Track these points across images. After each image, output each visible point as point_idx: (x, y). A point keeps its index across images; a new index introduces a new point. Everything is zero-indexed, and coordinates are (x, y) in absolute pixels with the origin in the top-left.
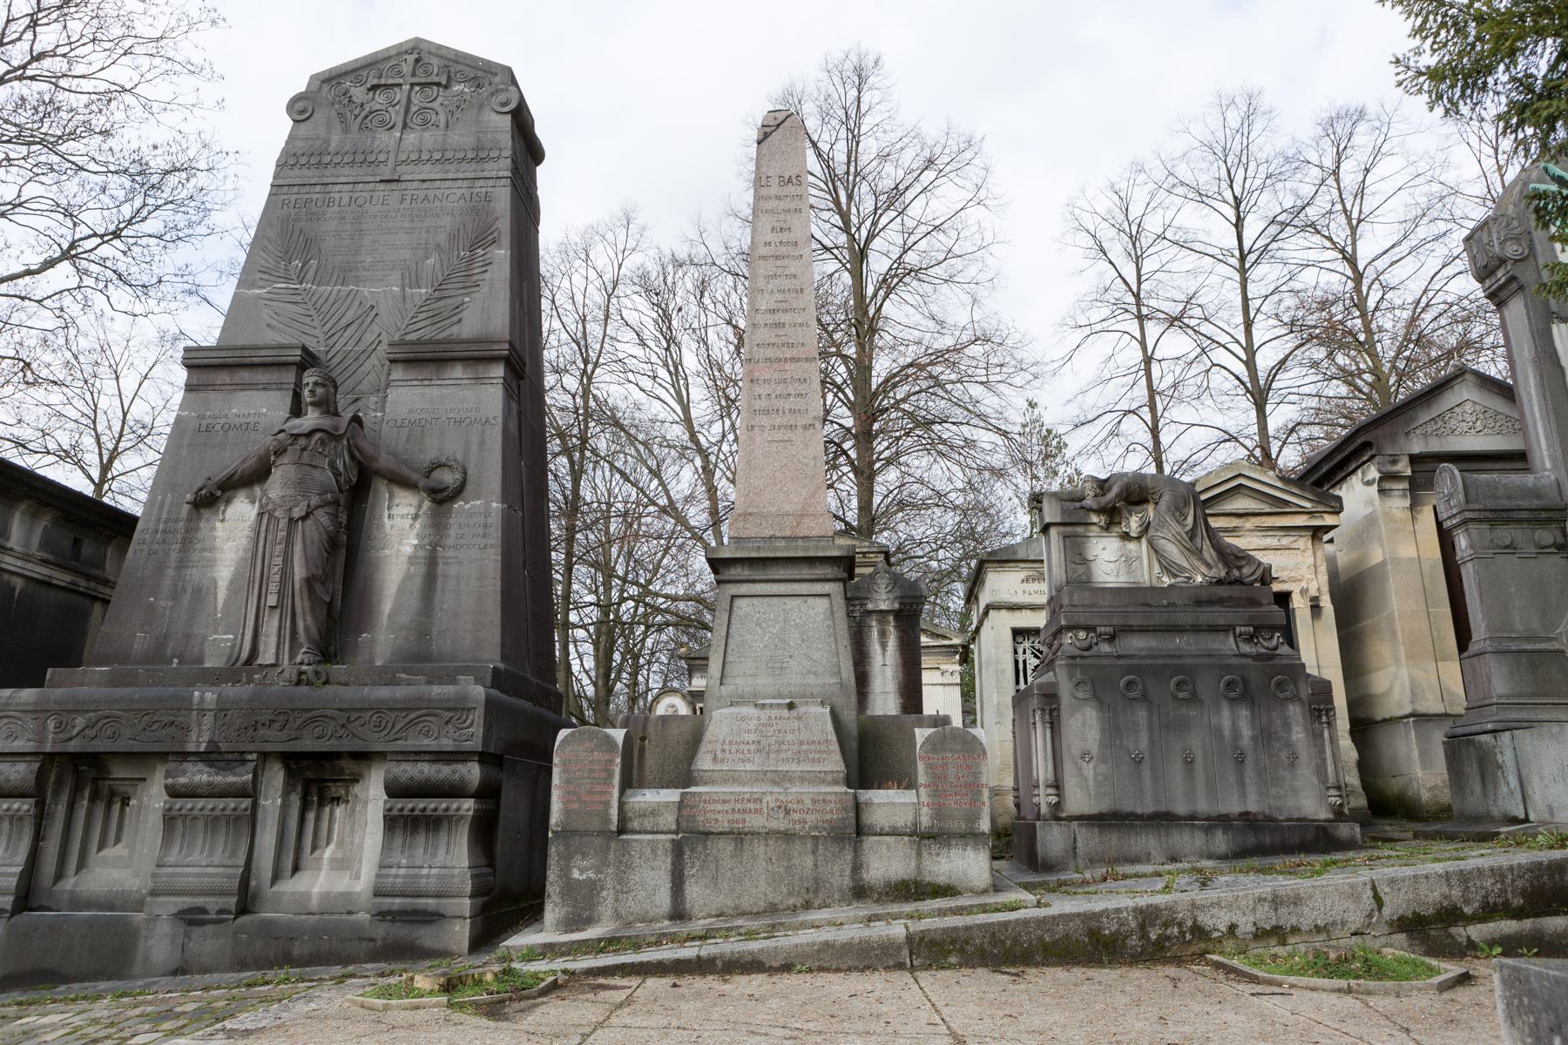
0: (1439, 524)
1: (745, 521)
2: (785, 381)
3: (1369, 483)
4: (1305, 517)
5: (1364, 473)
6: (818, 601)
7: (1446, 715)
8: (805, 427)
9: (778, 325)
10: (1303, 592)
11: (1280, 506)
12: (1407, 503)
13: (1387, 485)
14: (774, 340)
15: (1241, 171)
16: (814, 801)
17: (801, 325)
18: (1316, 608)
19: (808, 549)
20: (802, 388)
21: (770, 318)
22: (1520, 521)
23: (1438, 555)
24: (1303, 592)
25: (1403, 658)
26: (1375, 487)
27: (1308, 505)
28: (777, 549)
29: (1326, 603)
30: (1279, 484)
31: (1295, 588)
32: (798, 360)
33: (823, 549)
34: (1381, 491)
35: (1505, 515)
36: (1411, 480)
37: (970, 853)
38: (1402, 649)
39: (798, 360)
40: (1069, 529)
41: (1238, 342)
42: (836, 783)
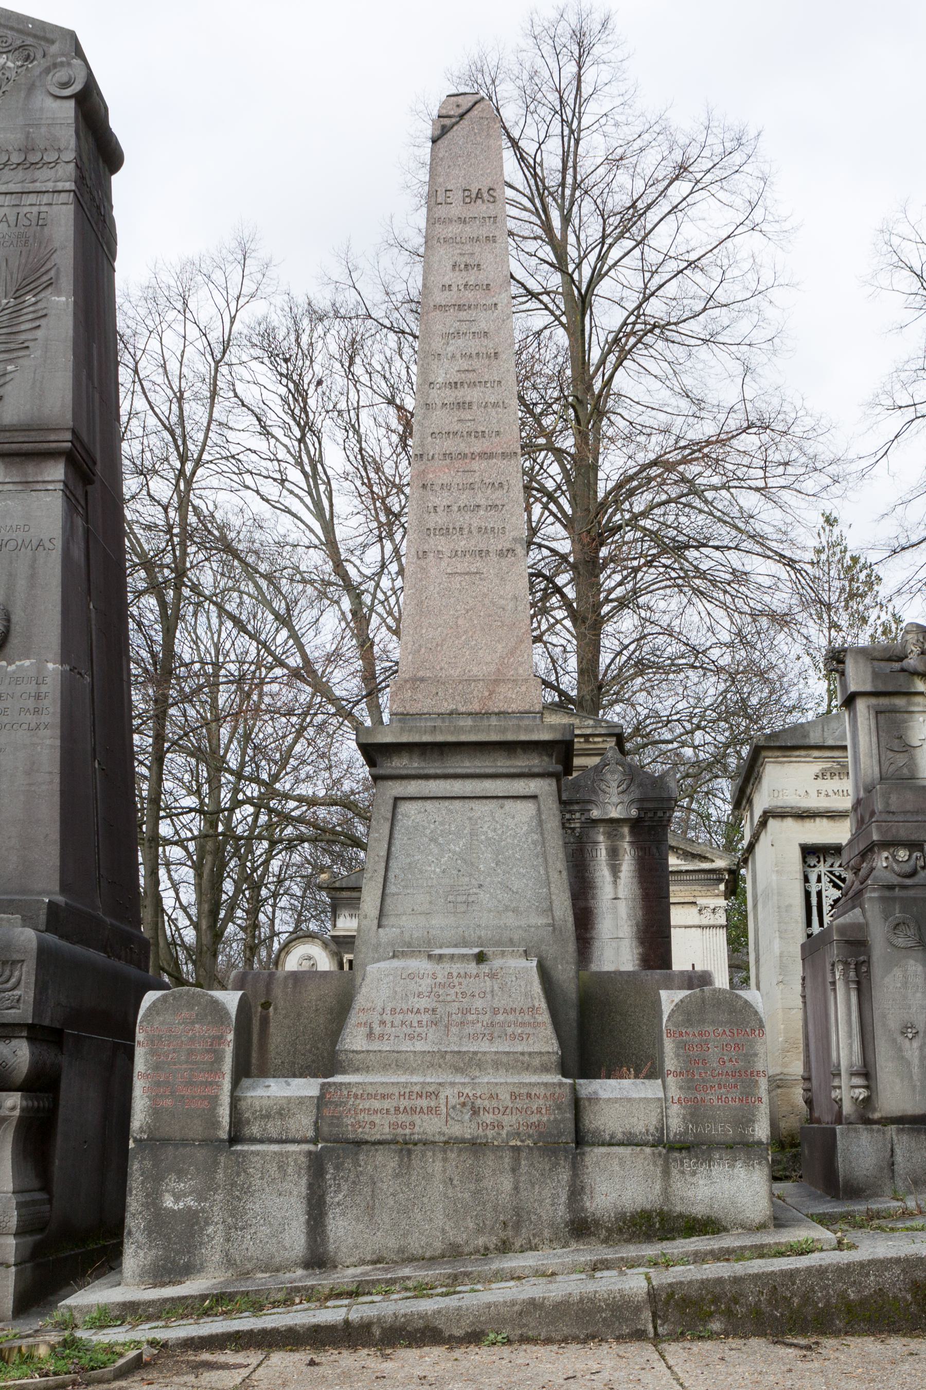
1: (414, 689)
6: (520, 805)
8: (501, 554)
9: (462, 405)
14: (456, 427)
17: (495, 405)
19: (504, 730)
20: (497, 496)
21: (450, 396)
28: (461, 730)
32: (491, 456)
37: (740, 1171)
39: (491, 456)
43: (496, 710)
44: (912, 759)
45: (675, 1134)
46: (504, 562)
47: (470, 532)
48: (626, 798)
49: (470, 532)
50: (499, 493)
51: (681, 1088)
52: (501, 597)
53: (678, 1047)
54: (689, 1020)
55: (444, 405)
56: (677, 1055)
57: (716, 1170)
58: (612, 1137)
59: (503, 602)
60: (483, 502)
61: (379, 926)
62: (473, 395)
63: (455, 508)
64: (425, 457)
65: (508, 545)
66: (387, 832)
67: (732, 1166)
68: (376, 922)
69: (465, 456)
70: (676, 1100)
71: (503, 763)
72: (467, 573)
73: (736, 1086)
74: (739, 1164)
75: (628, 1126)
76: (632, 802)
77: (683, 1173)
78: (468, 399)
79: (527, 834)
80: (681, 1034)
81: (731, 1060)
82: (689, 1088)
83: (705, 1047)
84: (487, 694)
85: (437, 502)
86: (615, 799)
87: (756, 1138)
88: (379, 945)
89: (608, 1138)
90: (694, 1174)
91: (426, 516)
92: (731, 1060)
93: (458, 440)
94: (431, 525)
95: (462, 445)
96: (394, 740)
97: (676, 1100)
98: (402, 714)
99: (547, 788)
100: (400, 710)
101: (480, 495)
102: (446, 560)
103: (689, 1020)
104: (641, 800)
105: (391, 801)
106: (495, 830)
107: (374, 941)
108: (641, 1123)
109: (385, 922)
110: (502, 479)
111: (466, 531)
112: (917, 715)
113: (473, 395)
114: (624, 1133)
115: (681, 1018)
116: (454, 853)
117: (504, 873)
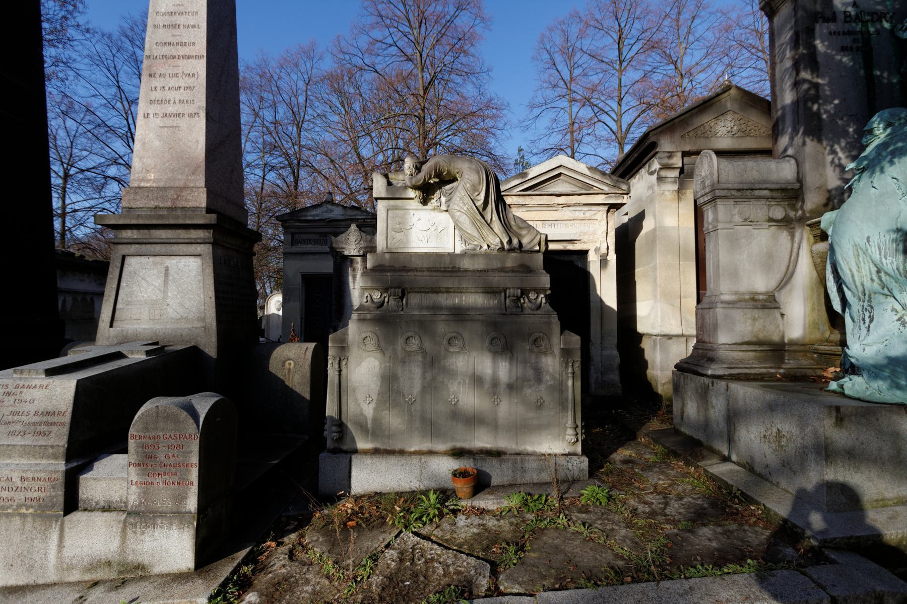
0: (695, 201)
1: (136, 193)
2: (176, 75)
3: (652, 173)
5: (649, 167)
7: (682, 335)
9: (176, 26)
10: (597, 250)
11: (587, 189)
12: (676, 187)
13: (664, 173)
14: (170, 40)
15: (626, 13)
16: (23, 479)
17: (194, 26)
18: (604, 262)
20: (190, 81)
21: (168, 20)
22: (759, 198)
23: (638, 271)
24: (597, 250)
26: (655, 176)
27: (606, 189)
28: (178, 217)
30: (587, 172)
31: (591, 247)
32: (189, 57)
36: (682, 171)
37: (174, 532)
39: (189, 57)
41: (613, 110)
42: (55, 457)
44: (406, 235)
46: (192, 120)
47: (175, 102)
48: (359, 246)
49: (175, 102)
50: (192, 79)
53: (138, 447)
54: (146, 428)
55: (164, 26)
57: (158, 531)
58: (97, 504)
61: (111, 326)
62: (181, 20)
63: (167, 88)
65: (196, 111)
66: (118, 274)
67: (169, 529)
69: (175, 57)
71: (182, 234)
74: (174, 527)
77: (135, 533)
78: (178, 23)
79: (195, 276)
81: (173, 456)
85: (157, 85)
86: (354, 247)
87: (187, 510)
89: (94, 504)
90: (143, 533)
92: (173, 456)
93: (171, 47)
94: (153, 98)
102: (160, 118)
103: (146, 428)
104: (366, 248)
105: (121, 258)
107: (107, 335)
108: (117, 495)
109: (115, 324)
111: (172, 102)
113: (181, 20)
116: (155, 286)
117: (182, 297)
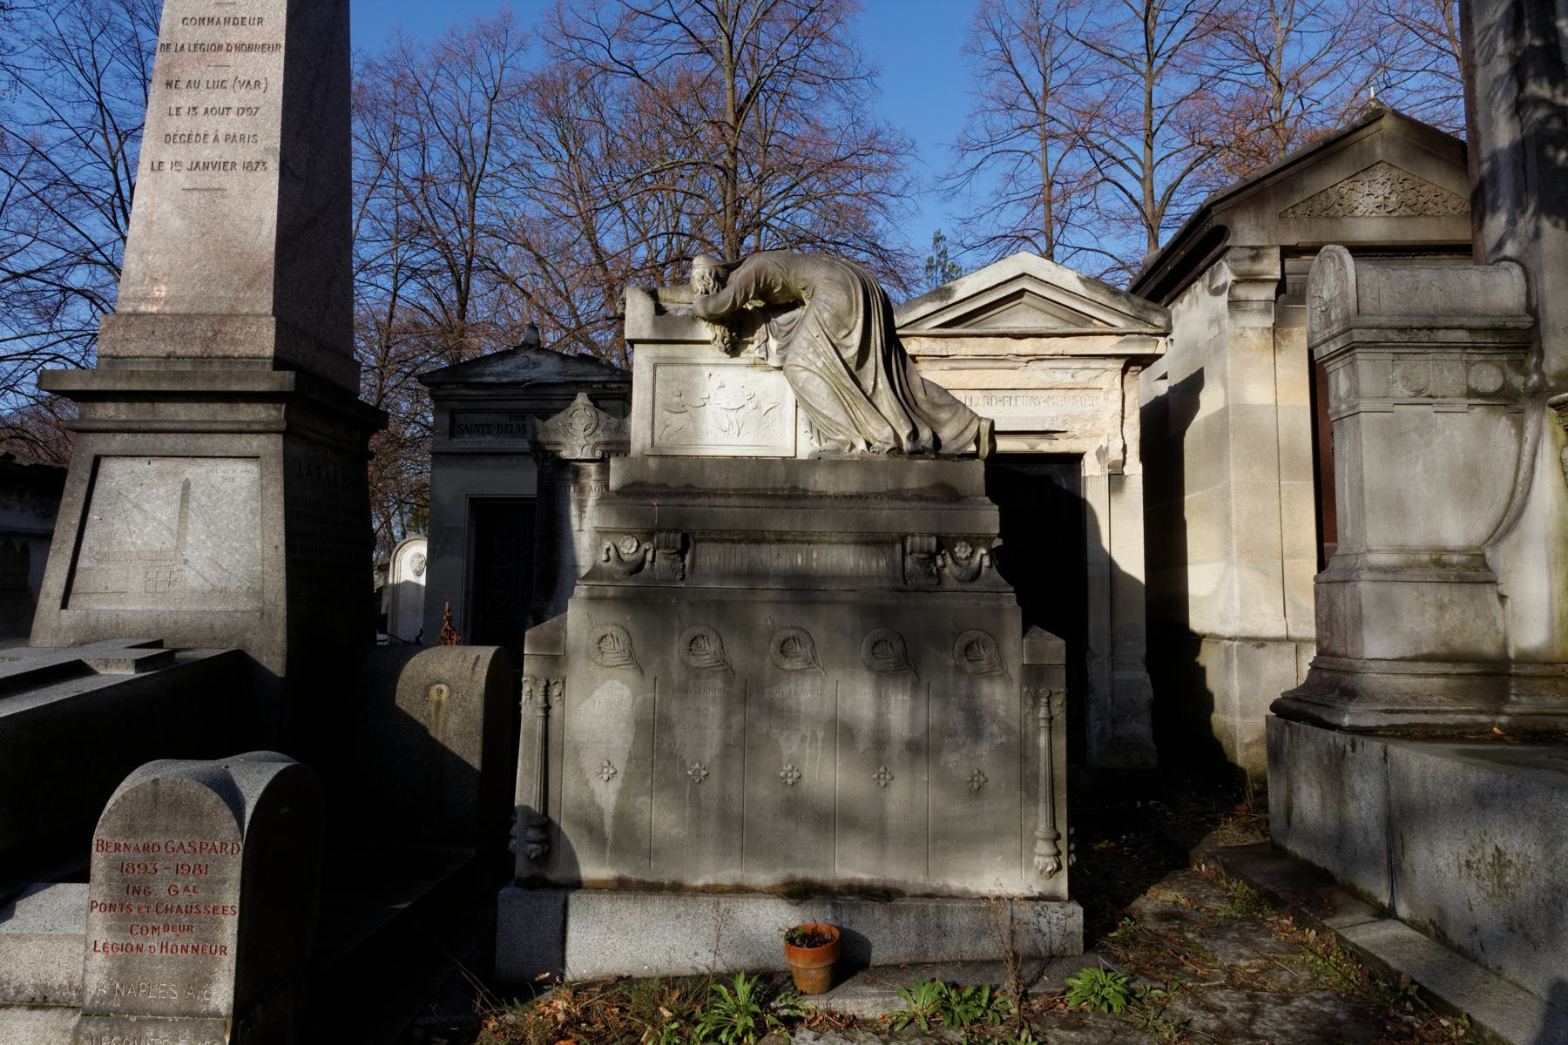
1: (128, 326)
3: (1217, 292)
4: (1114, 339)
5: (1212, 278)
6: (240, 466)
7: (1288, 639)
8: (248, 166)
10: (1102, 453)
11: (1079, 325)
12: (1269, 322)
13: (1242, 292)
18: (1116, 479)
19: (214, 378)
20: (250, 97)
22: (1446, 346)
24: (1102, 453)
25: (1235, 553)
26: (1225, 297)
27: (1120, 323)
28: (214, 378)
29: (1134, 470)
30: (1079, 288)
32: (250, 48)
33: (239, 379)
34: (1235, 304)
35: (1390, 577)
36: (1281, 287)
38: (1235, 540)
39: (250, 48)
40: (665, 350)
41: (1136, 157)
43: (220, 353)
44: (693, 419)
45: (94, 998)
46: (252, 176)
47: (216, 139)
48: (592, 441)
49: (216, 139)
50: (255, 93)
51: (109, 929)
52: (244, 219)
54: (131, 827)
56: (109, 880)
58: (18, 991)
59: (245, 225)
60: (235, 104)
64: (173, 48)
68: (59, 602)
69: (220, 47)
70: (100, 947)
72: (207, 190)
73: (190, 928)
75: (44, 976)
76: (598, 444)
79: (245, 501)
80: (117, 847)
81: (186, 889)
82: (121, 929)
83: (150, 868)
84: (210, 334)
87: (212, 1007)
88: (60, 629)
91: (167, 119)
92: (186, 889)
94: (172, 131)
95: (218, 34)
96: (84, 388)
97: (100, 947)
98: (112, 357)
99: (272, 447)
100: (109, 351)
101: (232, 94)
104: (607, 443)
106: (209, 496)
108: (63, 972)
110: (260, 77)
111: (211, 139)
112: (704, 369)
114: (35, 986)
115: (119, 823)
